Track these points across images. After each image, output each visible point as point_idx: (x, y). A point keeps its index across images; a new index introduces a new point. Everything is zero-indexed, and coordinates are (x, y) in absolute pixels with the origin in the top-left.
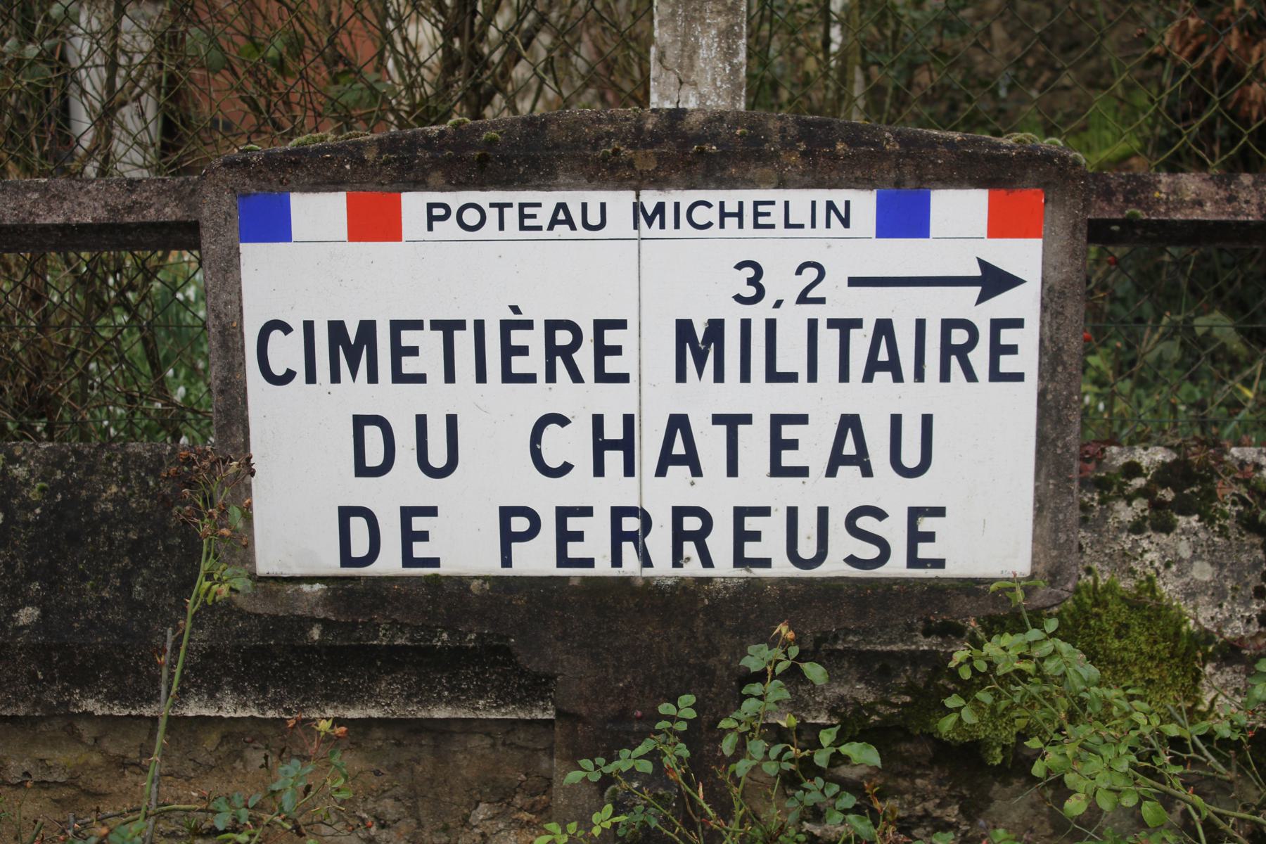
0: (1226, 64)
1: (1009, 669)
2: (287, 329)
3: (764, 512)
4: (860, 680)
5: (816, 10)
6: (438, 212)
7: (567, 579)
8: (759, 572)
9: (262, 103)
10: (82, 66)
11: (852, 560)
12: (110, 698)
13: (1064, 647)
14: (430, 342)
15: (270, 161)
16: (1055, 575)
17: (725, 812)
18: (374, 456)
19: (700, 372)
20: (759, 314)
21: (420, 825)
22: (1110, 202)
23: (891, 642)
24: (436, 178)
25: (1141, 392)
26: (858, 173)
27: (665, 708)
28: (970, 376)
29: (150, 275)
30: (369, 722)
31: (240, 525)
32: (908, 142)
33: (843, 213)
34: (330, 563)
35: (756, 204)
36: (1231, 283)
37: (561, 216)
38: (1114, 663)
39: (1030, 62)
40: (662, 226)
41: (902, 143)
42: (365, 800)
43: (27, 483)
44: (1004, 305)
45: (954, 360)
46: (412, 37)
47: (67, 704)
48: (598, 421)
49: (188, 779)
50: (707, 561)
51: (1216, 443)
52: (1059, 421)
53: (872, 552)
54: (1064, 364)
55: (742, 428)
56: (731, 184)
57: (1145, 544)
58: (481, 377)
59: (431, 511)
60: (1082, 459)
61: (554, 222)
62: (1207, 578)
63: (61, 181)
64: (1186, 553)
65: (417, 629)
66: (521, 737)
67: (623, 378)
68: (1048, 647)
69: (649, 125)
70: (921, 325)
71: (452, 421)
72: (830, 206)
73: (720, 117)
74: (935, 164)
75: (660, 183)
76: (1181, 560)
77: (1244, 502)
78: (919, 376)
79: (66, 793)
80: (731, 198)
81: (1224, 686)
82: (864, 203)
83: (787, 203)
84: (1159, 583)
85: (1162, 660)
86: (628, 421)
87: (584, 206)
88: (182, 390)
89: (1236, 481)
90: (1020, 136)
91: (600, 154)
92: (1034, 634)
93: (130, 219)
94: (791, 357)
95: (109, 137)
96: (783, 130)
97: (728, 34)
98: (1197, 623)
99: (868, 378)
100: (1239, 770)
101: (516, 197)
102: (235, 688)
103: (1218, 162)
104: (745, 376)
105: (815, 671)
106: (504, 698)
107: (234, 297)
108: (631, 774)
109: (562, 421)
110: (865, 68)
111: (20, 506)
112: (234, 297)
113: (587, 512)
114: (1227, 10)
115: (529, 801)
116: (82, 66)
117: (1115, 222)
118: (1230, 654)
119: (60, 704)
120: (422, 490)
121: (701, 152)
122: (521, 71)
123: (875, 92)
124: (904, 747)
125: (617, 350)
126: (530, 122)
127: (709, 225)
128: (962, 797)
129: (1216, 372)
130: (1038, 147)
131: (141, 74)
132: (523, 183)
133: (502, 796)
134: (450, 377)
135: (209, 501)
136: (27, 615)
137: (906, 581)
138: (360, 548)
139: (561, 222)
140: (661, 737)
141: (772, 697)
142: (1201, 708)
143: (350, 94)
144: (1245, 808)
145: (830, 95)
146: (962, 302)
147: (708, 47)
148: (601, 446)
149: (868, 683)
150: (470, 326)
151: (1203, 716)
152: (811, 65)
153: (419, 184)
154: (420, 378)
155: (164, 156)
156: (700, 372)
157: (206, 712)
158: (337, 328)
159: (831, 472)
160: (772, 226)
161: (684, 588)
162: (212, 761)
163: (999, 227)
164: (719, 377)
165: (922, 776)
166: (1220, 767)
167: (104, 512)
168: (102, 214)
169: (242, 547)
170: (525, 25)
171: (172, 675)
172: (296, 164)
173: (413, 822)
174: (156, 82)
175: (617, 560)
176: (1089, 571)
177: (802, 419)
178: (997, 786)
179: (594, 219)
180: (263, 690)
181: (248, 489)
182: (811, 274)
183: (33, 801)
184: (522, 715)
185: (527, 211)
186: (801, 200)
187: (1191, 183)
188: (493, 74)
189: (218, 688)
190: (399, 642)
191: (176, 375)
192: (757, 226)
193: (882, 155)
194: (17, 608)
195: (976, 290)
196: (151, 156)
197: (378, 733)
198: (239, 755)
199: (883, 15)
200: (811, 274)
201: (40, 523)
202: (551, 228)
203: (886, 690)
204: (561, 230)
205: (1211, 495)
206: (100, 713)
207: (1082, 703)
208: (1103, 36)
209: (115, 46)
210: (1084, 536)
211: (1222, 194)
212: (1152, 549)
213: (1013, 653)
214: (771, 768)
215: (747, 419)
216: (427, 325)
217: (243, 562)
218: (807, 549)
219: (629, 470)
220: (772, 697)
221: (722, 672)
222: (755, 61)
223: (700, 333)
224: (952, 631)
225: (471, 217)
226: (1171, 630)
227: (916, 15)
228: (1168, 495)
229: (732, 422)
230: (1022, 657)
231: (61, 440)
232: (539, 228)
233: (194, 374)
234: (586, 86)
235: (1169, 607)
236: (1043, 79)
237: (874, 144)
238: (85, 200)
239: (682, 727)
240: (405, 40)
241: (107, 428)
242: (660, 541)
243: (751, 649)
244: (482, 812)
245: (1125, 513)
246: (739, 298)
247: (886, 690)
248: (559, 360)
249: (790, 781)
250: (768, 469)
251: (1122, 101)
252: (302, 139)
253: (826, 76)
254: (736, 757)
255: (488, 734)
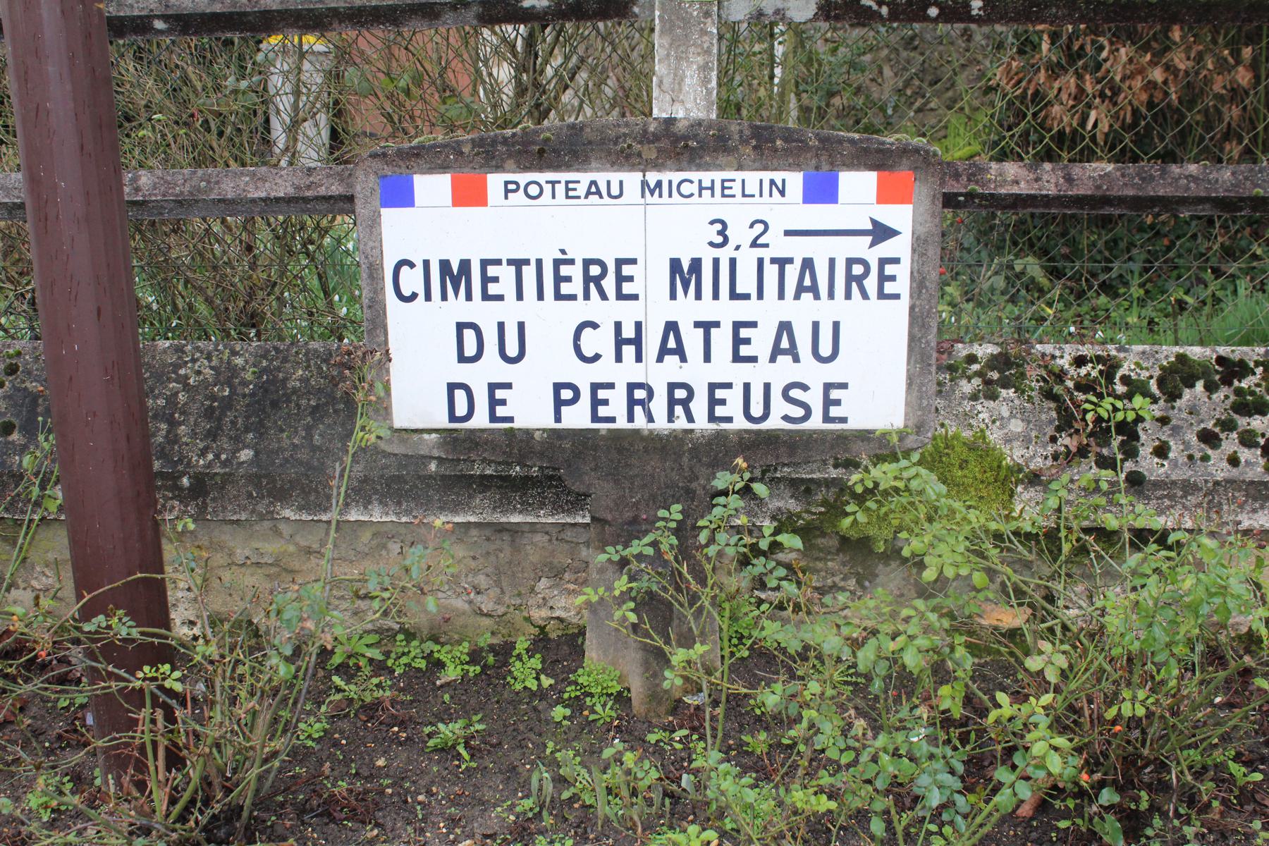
0: (1036, 93)
1: (887, 486)
2: (412, 265)
3: (728, 386)
4: (792, 497)
5: (765, 56)
6: (511, 187)
7: (597, 430)
8: (724, 426)
9: (396, 118)
10: (277, 94)
11: (786, 418)
12: (300, 508)
13: (923, 471)
14: (506, 274)
15: (401, 154)
16: (919, 428)
17: (702, 581)
18: (470, 350)
19: (686, 293)
20: (724, 255)
21: (503, 592)
22: (958, 181)
23: (812, 472)
24: (510, 163)
25: (980, 311)
26: (791, 161)
27: (662, 513)
28: (865, 296)
29: (324, 232)
30: (468, 525)
31: (382, 394)
32: (824, 140)
33: (780, 187)
34: (443, 421)
35: (723, 181)
36: (1039, 239)
37: (593, 189)
38: (958, 485)
39: (909, 92)
40: (660, 196)
41: (820, 140)
42: (467, 576)
43: (244, 369)
44: (887, 248)
45: (854, 285)
46: (495, 74)
47: (272, 512)
48: (618, 326)
49: (352, 562)
50: (690, 419)
51: (1027, 342)
52: (923, 326)
53: (798, 412)
54: (926, 288)
55: (713, 331)
56: (707, 167)
57: (979, 408)
58: (540, 296)
59: (508, 386)
60: (939, 352)
61: (589, 193)
62: (1019, 430)
63: (264, 169)
64: (1006, 413)
65: (499, 463)
66: (568, 534)
67: (635, 297)
68: (913, 471)
69: (652, 129)
70: (832, 262)
71: (521, 326)
72: (772, 182)
73: (699, 123)
74: (842, 155)
75: (658, 166)
76: (1002, 418)
77: (1044, 380)
78: (831, 295)
79: (273, 570)
80: (706, 177)
81: (1030, 500)
82: (795, 181)
83: (743, 181)
84: (988, 433)
85: (989, 484)
86: (638, 325)
87: (609, 183)
88: (344, 310)
89: (1040, 366)
90: (898, 136)
91: (618, 148)
92: (904, 463)
93: (309, 194)
94: (746, 283)
95: (296, 140)
96: (741, 131)
97: (705, 68)
98: (1013, 459)
99: (797, 297)
100: (1038, 554)
101: (563, 176)
102: (381, 502)
103: (1032, 152)
104: (716, 296)
105: (760, 489)
106: (557, 508)
107: (377, 244)
108: (640, 557)
109: (595, 326)
110: (798, 95)
111: (240, 383)
112: (377, 244)
113: (611, 386)
114: (1037, 56)
115: (573, 577)
116: (277, 94)
117: (961, 194)
118: (1034, 479)
119: (268, 512)
120: (503, 372)
121: (686, 146)
122: (567, 97)
123: (805, 110)
124: (820, 541)
125: (630, 279)
126: (573, 126)
127: (692, 195)
128: (858, 574)
129: (1029, 298)
130: (909, 144)
131: (317, 99)
132: (568, 167)
133: (557, 574)
134: (520, 296)
135: (362, 379)
136: (246, 455)
137: (822, 431)
138: (461, 410)
139: (593, 193)
140: (659, 532)
141: (732, 506)
142: (1014, 514)
143: (453, 110)
144: (1041, 579)
145: (774, 111)
146: (859, 245)
147: (691, 78)
148: (620, 342)
149: (796, 499)
150: (533, 263)
151: (1015, 519)
152: (762, 92)
153: (499, 168)
154: (500, 298)
155: (332, 153)
156: (686, 293)
157: (362, 518)
158: (445, 265)
159: (773, 359)
160: (733, 196)
161: (676, 437)
162: (366, 550)
163: (884, 197)
164: (698, 296)
165: (832, 560)
166: (1025, 553)
167: (294, 388)
168: (291, 191)
169: (383, 409)
170: (570, 65)
171: (339, 494)
172: (417, 155)
173: (498, 591)
174: (326, 106)
175: (631, 418)
176: (942, 425)
177: (753, 325)
178: (881, 567)
179: (615, 191)
180: (399, 503)
181: (388, 371)
182: (760, 228)
183: (252, 575)
184: (569, 520)
185: (571, 186)
186: (753, 178)
187: (1011, 169)
188: (549, 98)
189: (370, 502)
190: (488, 472)
191: (340, 300)
192: (723, 196)
193: (809, 149)
194: (239, 450)
195: (869, 239)
196: (324, 153)
197: (474, 532)
198: (384, 547)
199: (810, 60)
200: (760, 228)
201: (253, 395)
202: (586, 197)
203: (809, 504)
204: (594, 199)
205: (1023, 375)
206: (293, 518)
207: (936, 510)
208: (956, 74)
209: (299, 80)
210: (940, 403)
211: (1032, 176)
212: (984, 410)
213: (890, 475)
214: (731, 551)
215: (717, 324)
216: (504, 262)
217: (385, 419)
218: (757, 411)
219: (639, 358)
220: (732, 506)
221: (700, 492)
222: (724, 88)
223: (686, 267)
224: (851, 464)
225: (534, 190)
226: (995, 464)
227: (832, 59)
228: (995, 375)
229: (707, 327)
230: (896, 478)
231: (266, 340)
232: (578, 197)
233: (353, 300)
234: (613, 107)
235: (994, 449)
236: (917, 104)
237: (801, 141)
238: (279, 181)
239: (673, 525)
240: (490, 75)
241: (296, 335)
242: (659, 405)
243: (719, 475)
244: (544, 583)
245: (966, 387)
246: (712, 244)
247: (809, 504)
248: (592, 285)
249: (744, 562)
250: (731, 358)
251: (970, 119)
252: (422, 139)
253: (771, 98)
254: (707, 545)
255: (547, 533)
